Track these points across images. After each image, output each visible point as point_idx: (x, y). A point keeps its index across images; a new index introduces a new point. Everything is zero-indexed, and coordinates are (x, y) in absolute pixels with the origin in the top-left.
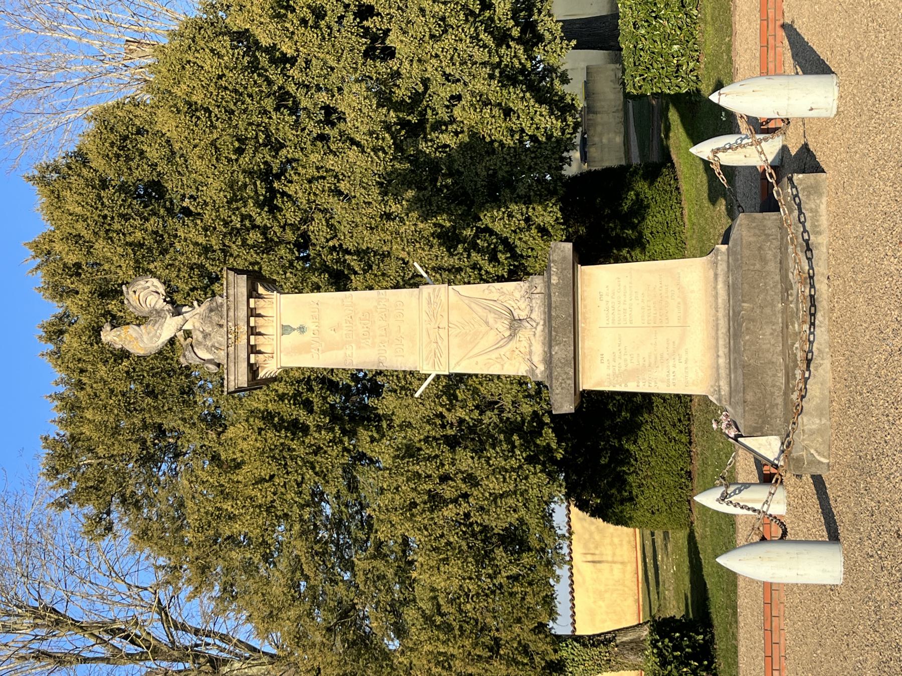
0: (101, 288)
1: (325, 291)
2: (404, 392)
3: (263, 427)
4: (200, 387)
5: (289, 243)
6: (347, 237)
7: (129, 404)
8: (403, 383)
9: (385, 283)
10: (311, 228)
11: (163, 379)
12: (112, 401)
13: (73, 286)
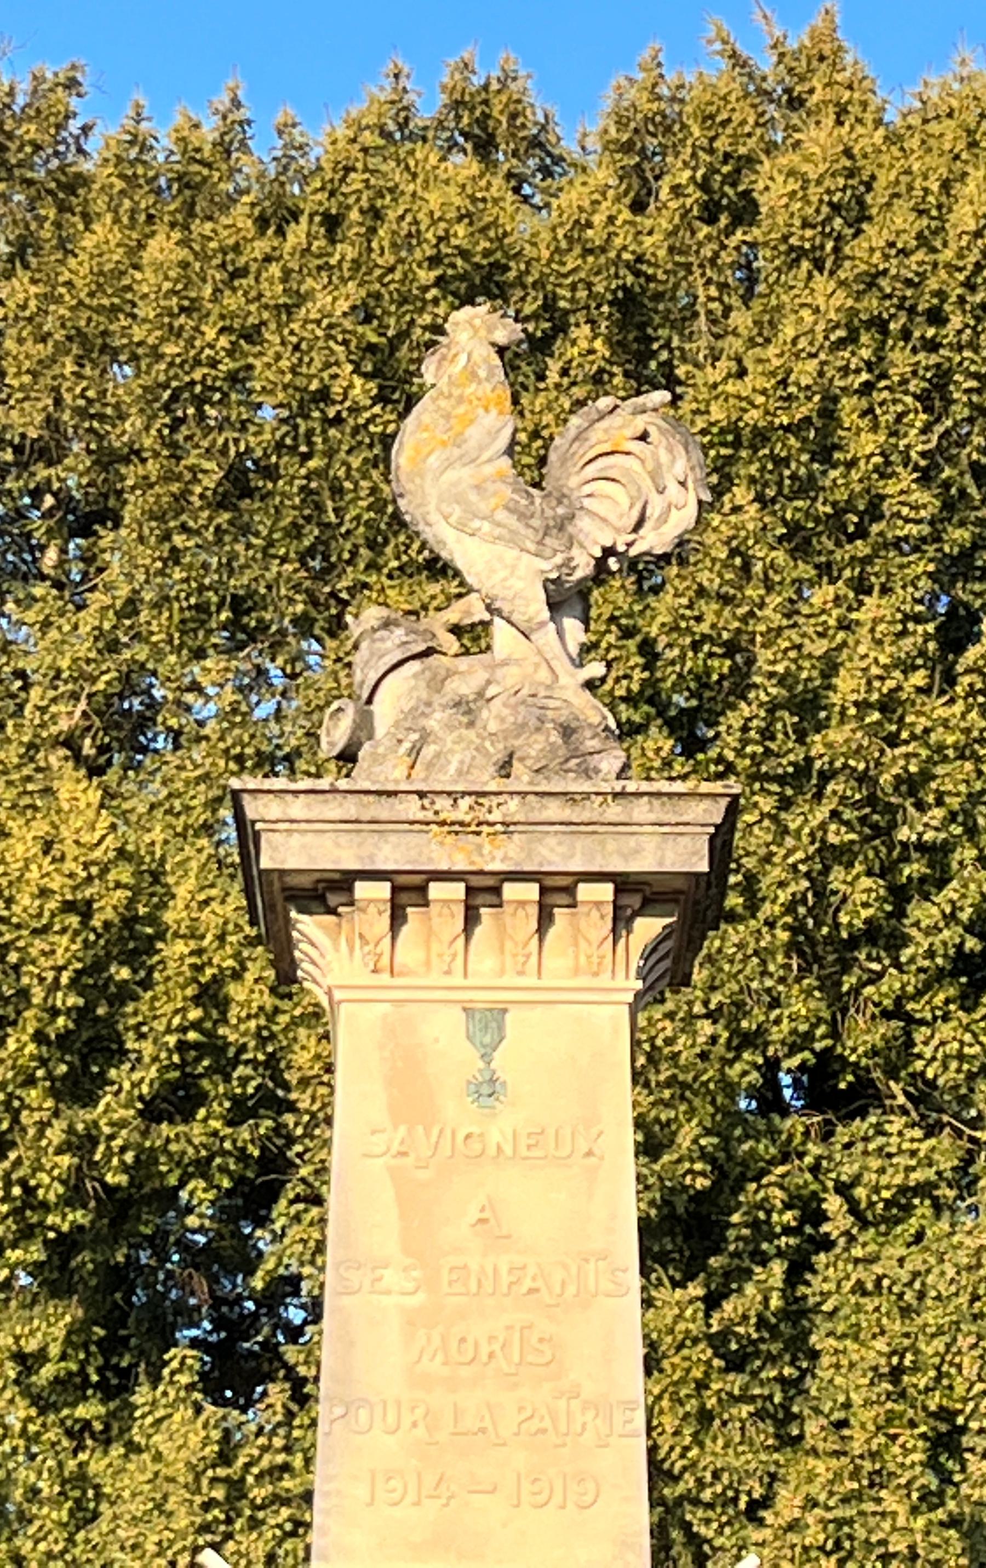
0: (658, 297)
1: (639, 1178)
2: (219, 1493)
3: (96, 922)
4: (261, 672)
5: (834, 1034)
6: (859, 1273)
7: (200, 402)
8: (259, 1493)
9: (669, 1422)
10: (896, 1124)
11: (295, 532)
12: (211, 334)
13: (664, 194)
